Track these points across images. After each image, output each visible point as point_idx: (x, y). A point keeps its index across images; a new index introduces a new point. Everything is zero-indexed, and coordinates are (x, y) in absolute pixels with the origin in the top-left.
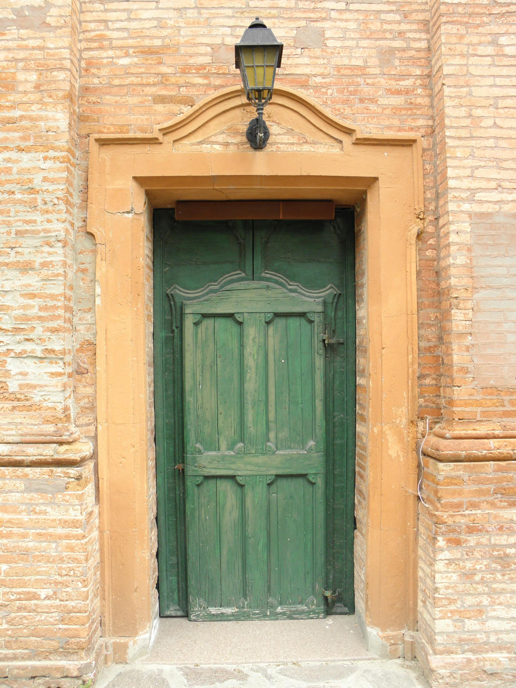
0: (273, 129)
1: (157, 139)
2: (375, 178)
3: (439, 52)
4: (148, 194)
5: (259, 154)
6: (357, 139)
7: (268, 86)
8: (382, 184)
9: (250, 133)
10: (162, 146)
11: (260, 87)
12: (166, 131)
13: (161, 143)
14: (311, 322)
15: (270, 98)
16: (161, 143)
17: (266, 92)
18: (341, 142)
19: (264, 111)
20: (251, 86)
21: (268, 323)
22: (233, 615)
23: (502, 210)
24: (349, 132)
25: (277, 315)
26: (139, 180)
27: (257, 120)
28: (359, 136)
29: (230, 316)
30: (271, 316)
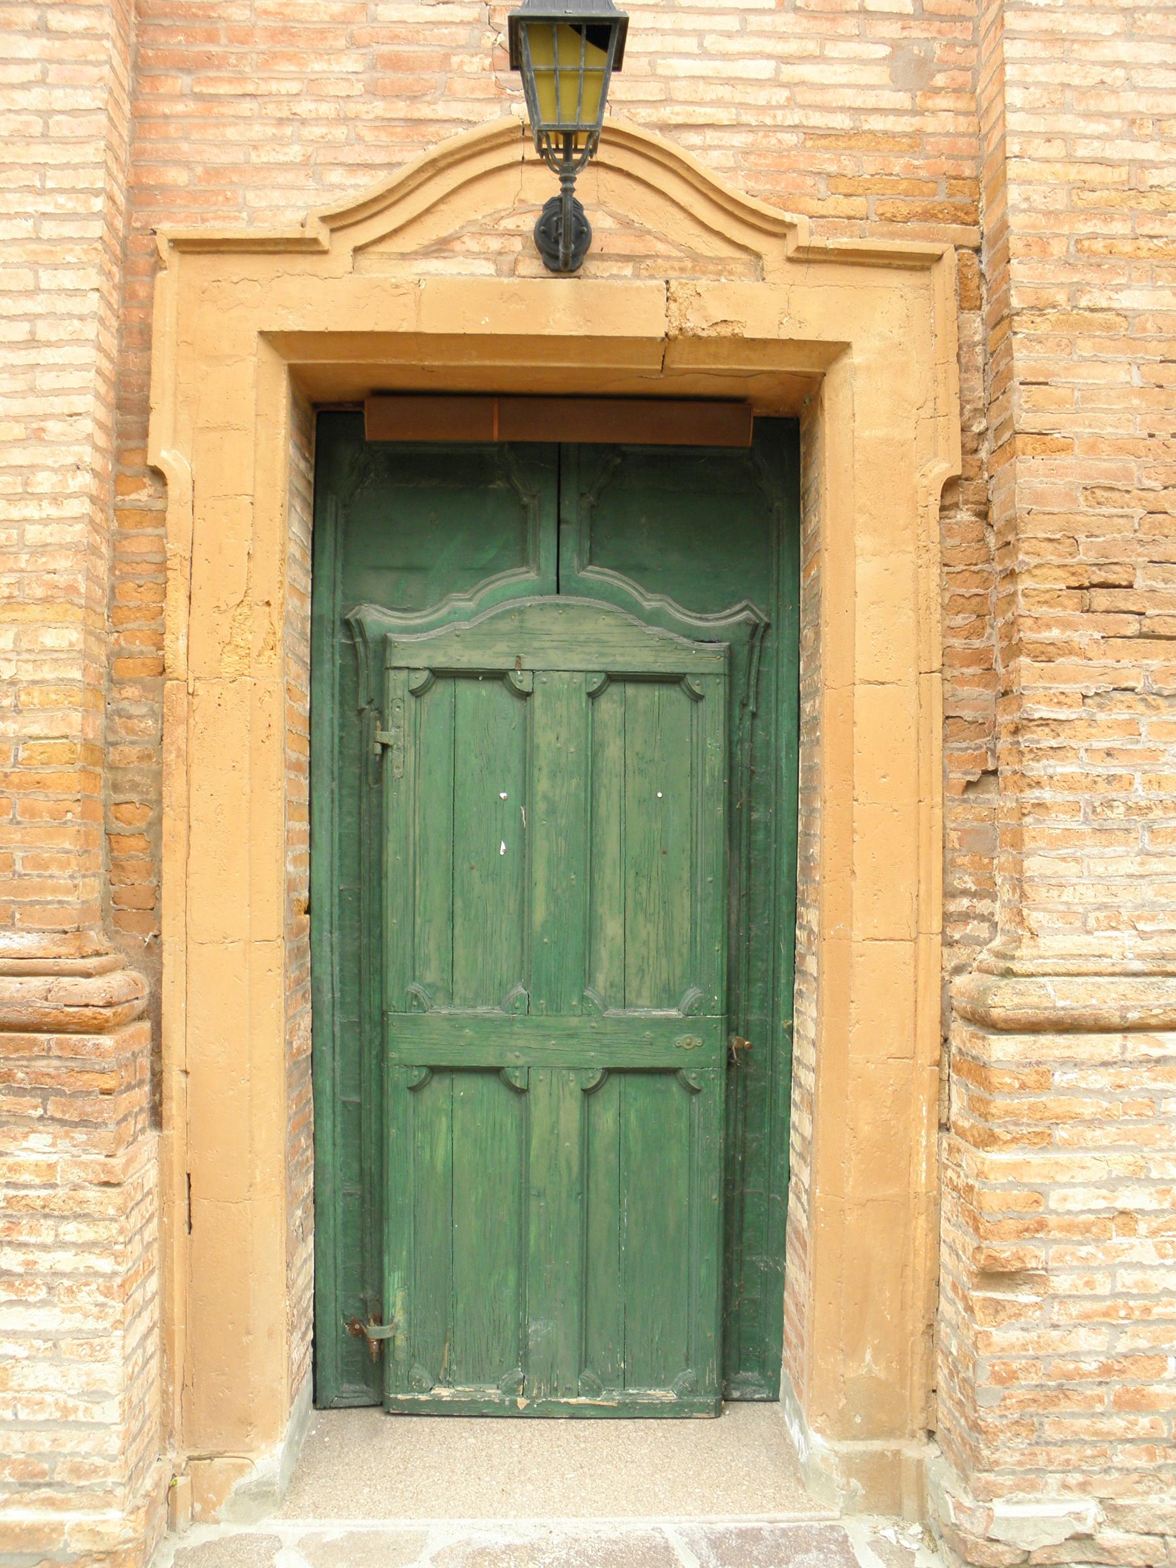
0: (598, 220)
1: (315, 241)
2: (844, 343)
3: (999, 128)
4: (297, 375)
5: (562, 286)
6: (799, 249)
7: (587, 121)
8: (856, 358)
9: (544, 232)
10: (324, 257)
11: (569, 123)
12: (338, 221)
13: (325, 252)
14: (697, 698)
15: (593, 151)
16: (325, 252)
17: (583, 137)
18: (758, 256)
19: (575, 185)
20: (547, 118)
21: (593, 696)
22: (672, 1405)
23: (1100, 1520)
24: (778, 230)
25: (613, 678)
26: (275, 340)
27: (559, 199)
28: (804, 241)
29: (497, 676)
30: (598, 680)
